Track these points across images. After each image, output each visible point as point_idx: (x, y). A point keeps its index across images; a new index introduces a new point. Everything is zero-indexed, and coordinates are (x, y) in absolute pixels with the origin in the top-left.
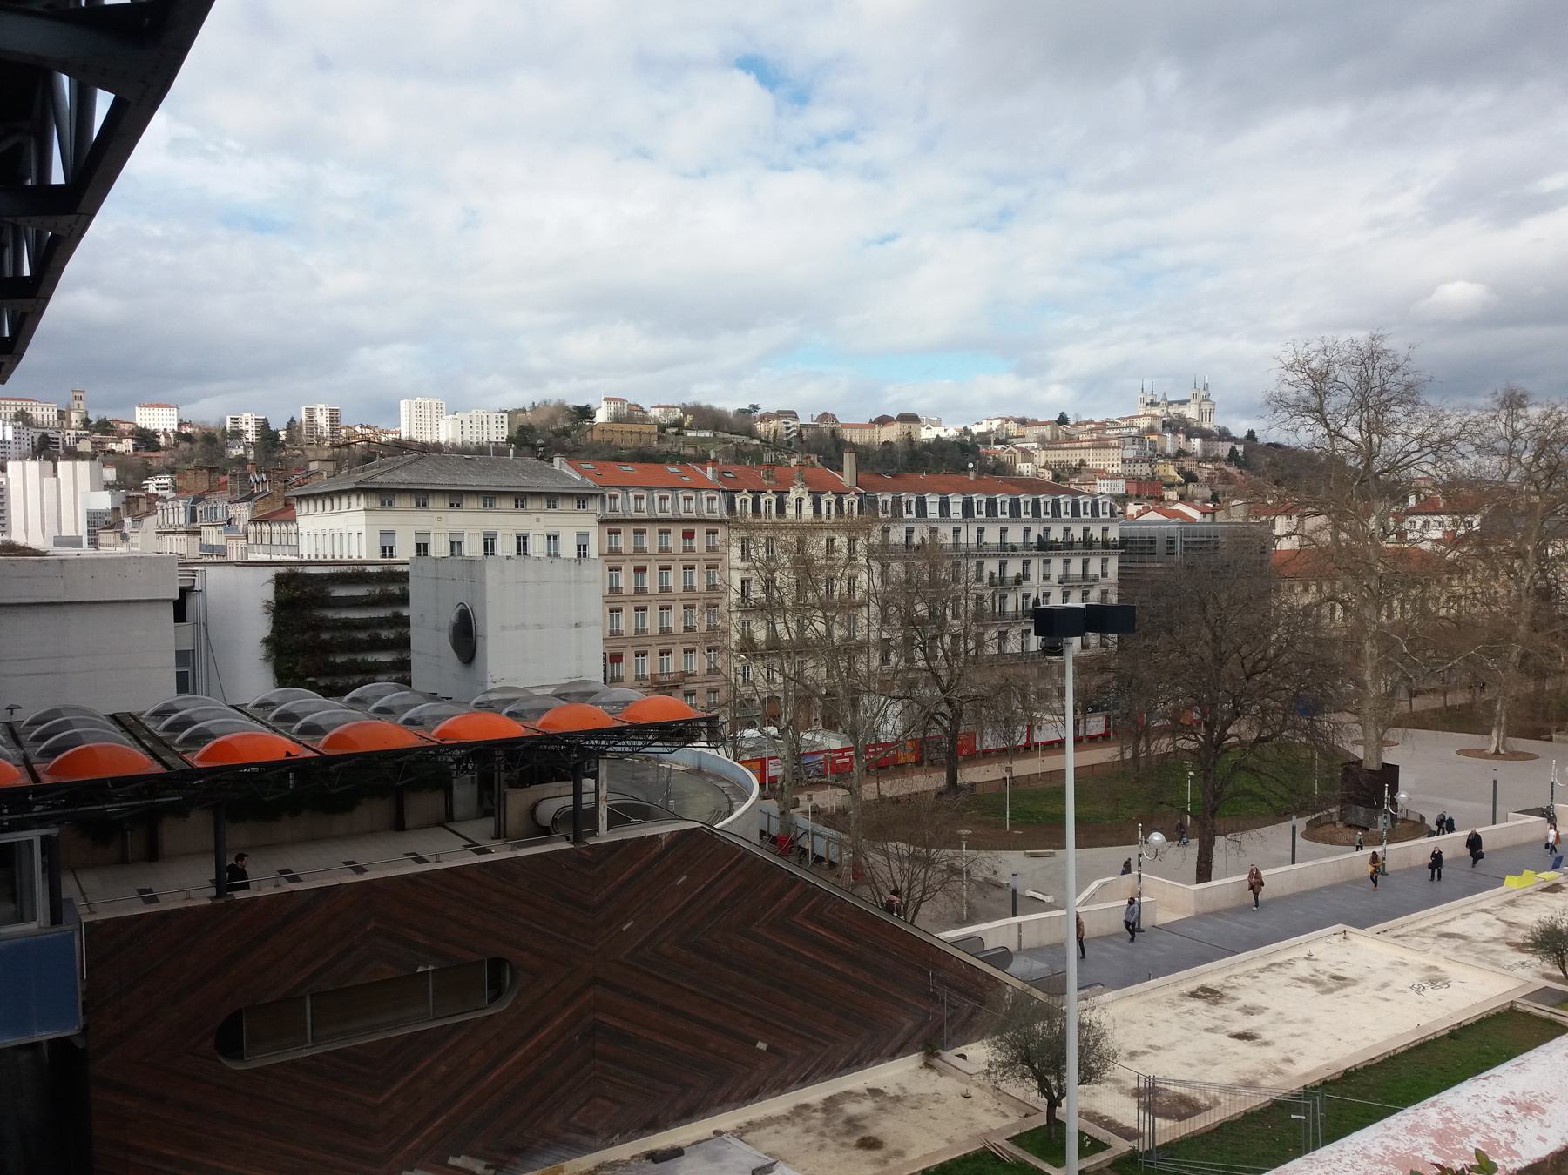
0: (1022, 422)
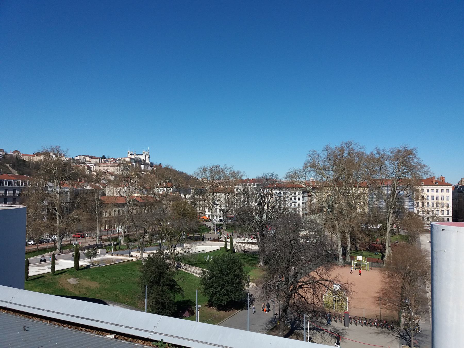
0: (91, 157)
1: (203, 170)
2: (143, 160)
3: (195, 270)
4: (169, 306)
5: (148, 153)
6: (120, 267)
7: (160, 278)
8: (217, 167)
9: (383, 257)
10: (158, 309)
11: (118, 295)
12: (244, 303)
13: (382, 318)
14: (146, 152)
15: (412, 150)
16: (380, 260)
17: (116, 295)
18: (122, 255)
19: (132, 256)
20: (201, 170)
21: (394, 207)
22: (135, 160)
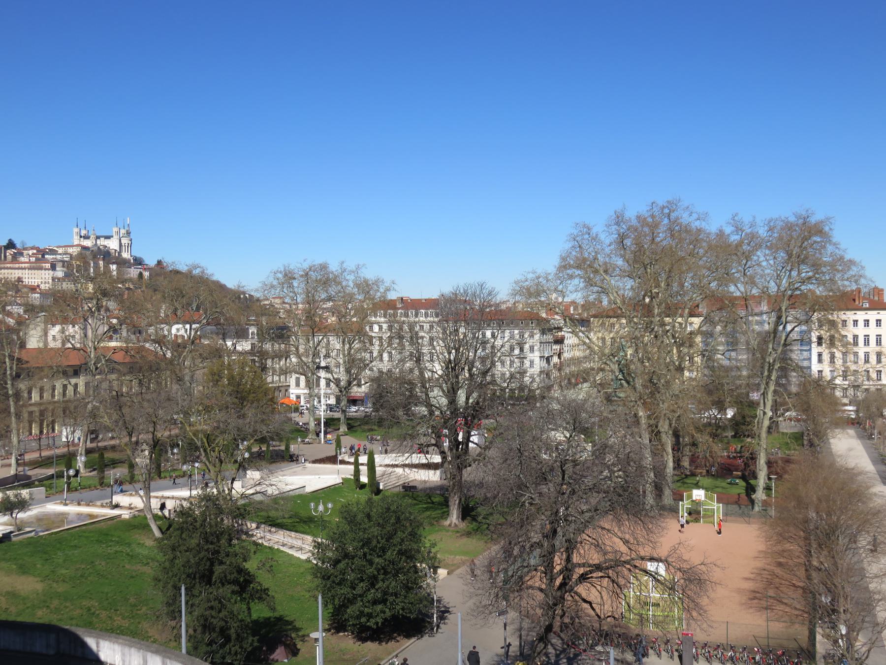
1: (284, 277)
2: (116, 250)
3: (286, 539)
4: (238, 635)
5: (128, 233)
6: (92, 534)
7: (212, 564)
8: (324, 267)
9: (751, 489)
10: (210, 644)
11: (93, 610)
12: (423, 621)
13: (772, 643)
14: (123, 231)
15: (822, 222)
16: (743, 496)
17: (89, 610)
18: (91, 502)
19: (117, 506)
20: (280, 276)
21: (779, 365)
22: (92, 251)
